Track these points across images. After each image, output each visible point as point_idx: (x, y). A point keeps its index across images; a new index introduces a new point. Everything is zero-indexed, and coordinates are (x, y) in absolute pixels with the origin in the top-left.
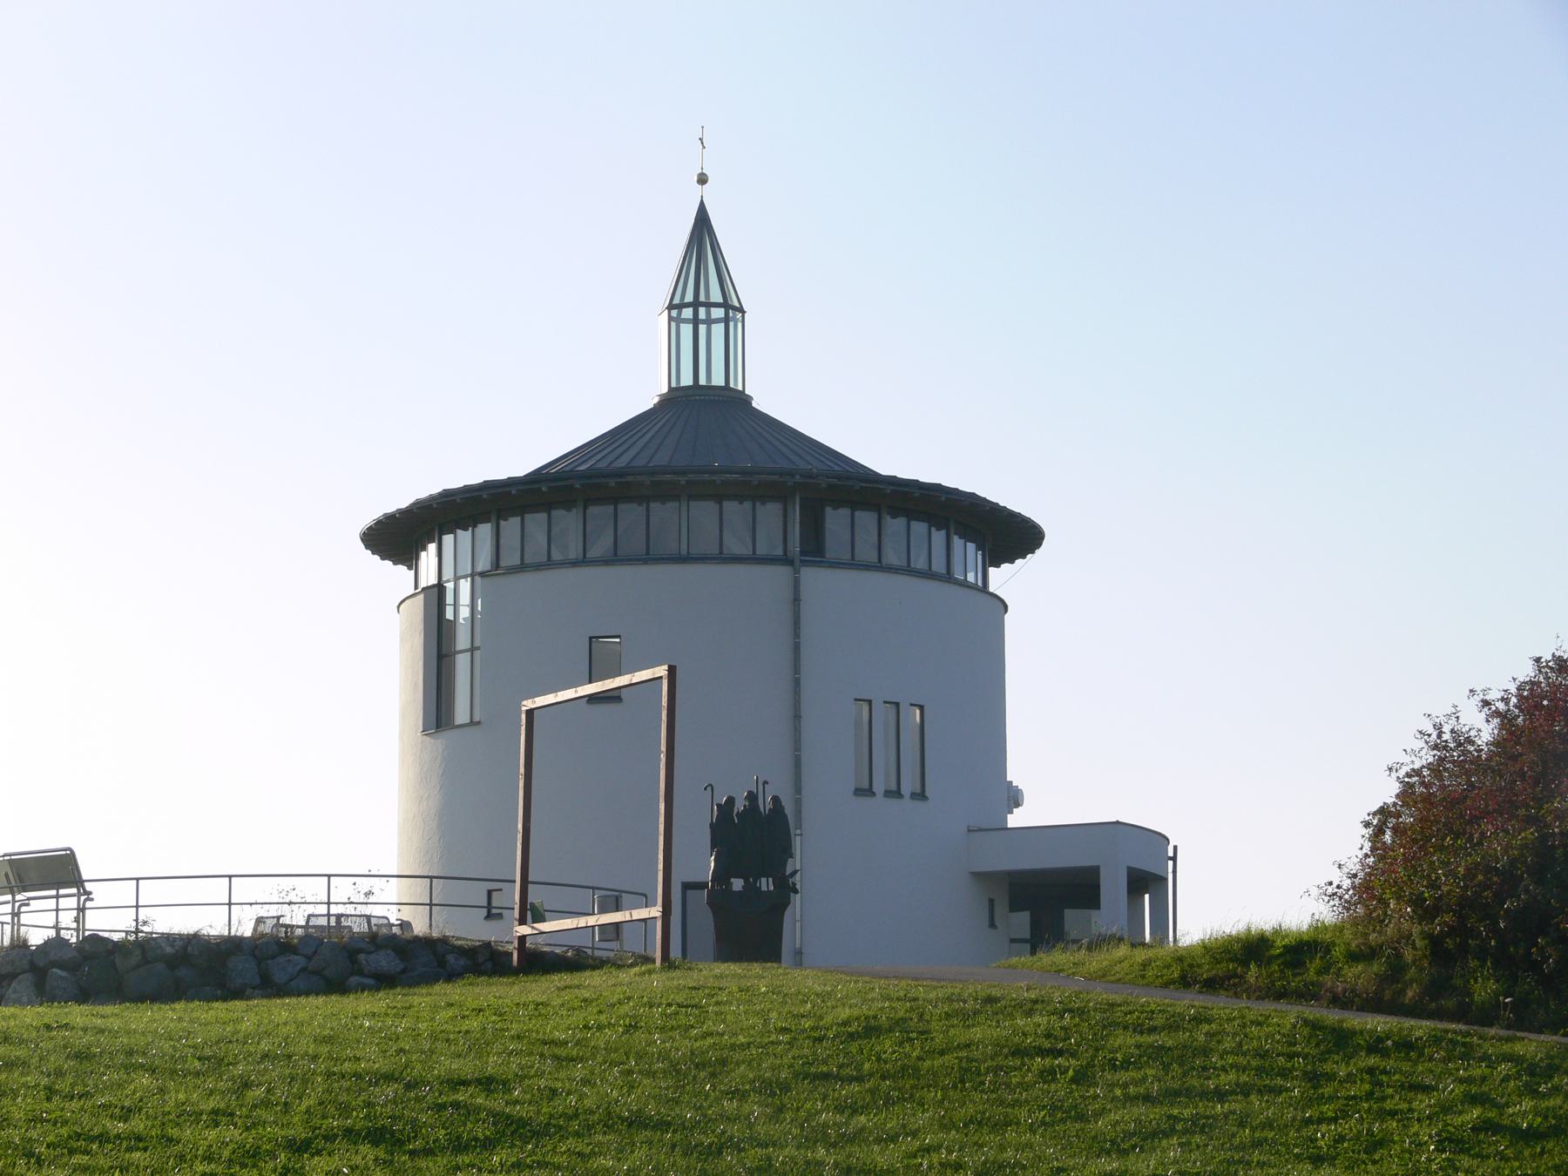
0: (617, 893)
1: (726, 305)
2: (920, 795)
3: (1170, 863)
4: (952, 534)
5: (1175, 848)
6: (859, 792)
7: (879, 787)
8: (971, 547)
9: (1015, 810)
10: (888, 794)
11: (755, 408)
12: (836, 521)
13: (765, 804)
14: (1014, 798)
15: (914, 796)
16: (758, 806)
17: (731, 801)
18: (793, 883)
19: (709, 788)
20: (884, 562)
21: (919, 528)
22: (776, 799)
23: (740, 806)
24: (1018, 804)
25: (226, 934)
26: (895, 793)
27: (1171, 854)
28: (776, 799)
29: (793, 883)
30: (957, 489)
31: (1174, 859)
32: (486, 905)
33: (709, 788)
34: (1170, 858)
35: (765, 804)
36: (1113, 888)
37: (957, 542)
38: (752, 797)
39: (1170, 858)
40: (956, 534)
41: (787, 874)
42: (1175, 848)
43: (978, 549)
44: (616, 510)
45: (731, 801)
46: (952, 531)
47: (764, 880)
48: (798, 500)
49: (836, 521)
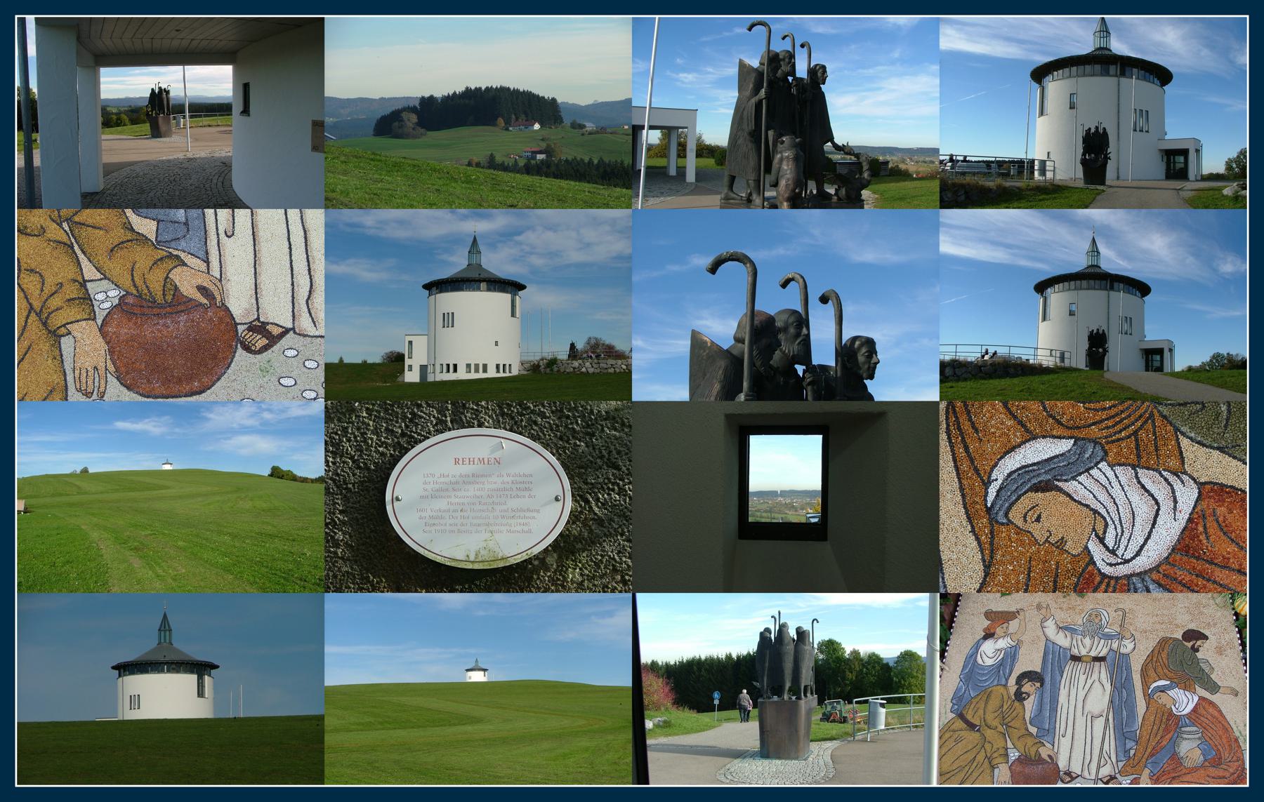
2: (1147, 132)
12: (1116, 285)
15: (1146, 131)
17: (1090, 129)
23: (1093, 130)
26: (1141, 131)
28: (1104, 129)
49: (1116, 285)
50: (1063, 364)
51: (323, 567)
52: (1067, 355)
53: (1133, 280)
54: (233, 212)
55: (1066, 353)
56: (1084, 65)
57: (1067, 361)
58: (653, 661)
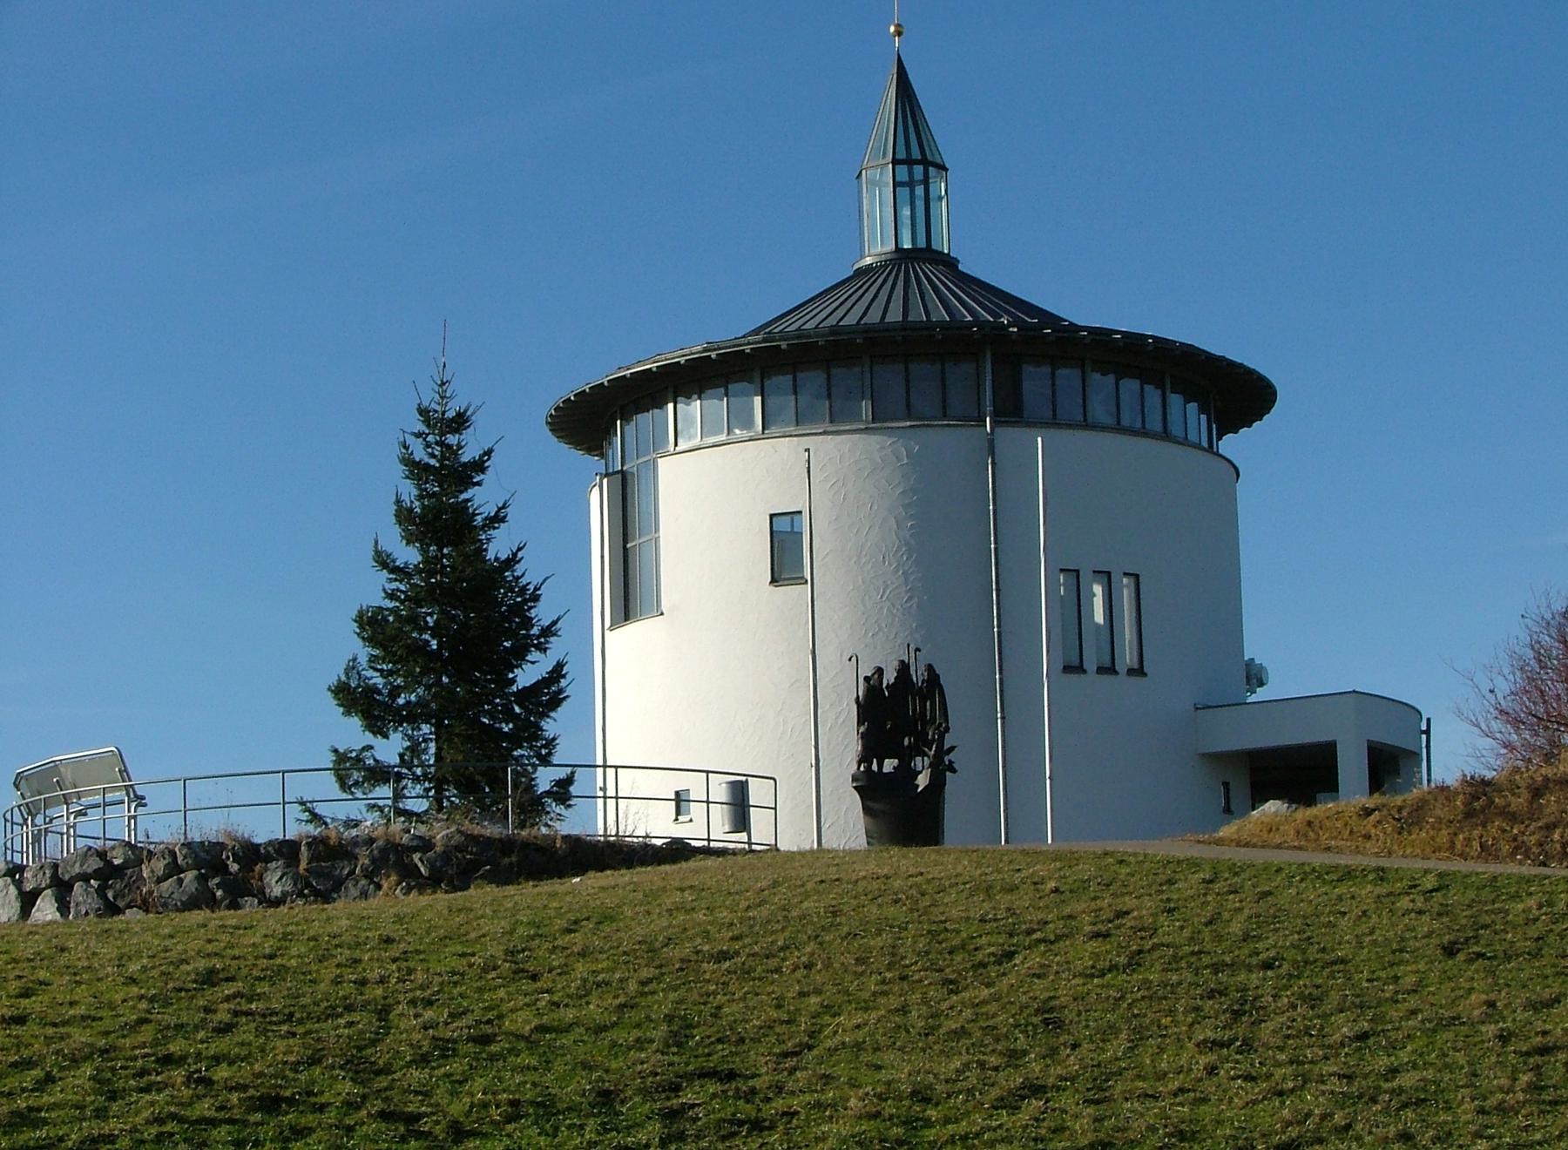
0: (744, 778)
1: (925, 163)
2: (1138, 671)
3: (1424, 737)
4: (1168, 394)
5: (1429, 720)
6: (1067, 669)
7: (1090, 664)
8: (1193, 407)
9: (1258, 689)
10: (1101, 670)
11: (963, 273)
12: (1034, 381)
13: (918, 675)
14: (1255, 677)
15: (1131, 672)
16: (910, 675)
17: (880, 671)
18: (950, 761)
19: (854, 659)
20: (1090, 420)
21: (1130, 386)
22: (930, 668)
23: (890, 677)
24: (1261, 684)
25: (281, 837)
26: (1109, 669)
27: (1424, 728)
28: (930, 668)
29: (950, 761)
30: (1268, 413)
31: (1427, 732)
32: (682, 803)
33: (854, 659)
34: (1423, 732)
35: (918, 675)
36: (1352, 768)
37: (1175, 400)
38: (904, 668)
39: (1423, 732)
40: (1172, 392)
41: (945, 748)
42: (1429, 720)
43: (1202, 410)
44: (795, 380)
45: (880, 671)
46: (1168, 386)
47: (919, 759)
48: (989, 356)
49: (1034, 381)
50: (743, 836)
51: (56, 848)
52: (758, 793)
53: (1134, 342)
54: (907, 370)
55: (753, 784)
56: (820, 853)
57: (760, 821)
58: (408, 543)
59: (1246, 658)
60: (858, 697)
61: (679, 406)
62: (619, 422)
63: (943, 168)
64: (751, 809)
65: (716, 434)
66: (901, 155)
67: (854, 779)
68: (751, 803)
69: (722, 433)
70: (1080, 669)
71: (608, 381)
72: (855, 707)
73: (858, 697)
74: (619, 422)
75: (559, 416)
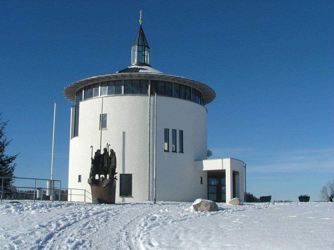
3: (244, 168)
5: (246, 164)
7: (170, 150)
23: (102, 152)
31: (245, 167)
34: (244, 167)
39: (244, 167)
42: (246, 164)
59: (208, 150)
60: (92, 158)
61: (102, 87)
62: (83, 91)
63: (148, 47)
64: (215, 192)
65: (105, 95)
66: (140, 44)
67: (88, 181)
68: (69, 188)
69: (106, 94)
70: (176, 151)
71: (78, 82)
72: (91, 160)
73: (92, 158)
74: (83, 91)
75: (68, 89)
